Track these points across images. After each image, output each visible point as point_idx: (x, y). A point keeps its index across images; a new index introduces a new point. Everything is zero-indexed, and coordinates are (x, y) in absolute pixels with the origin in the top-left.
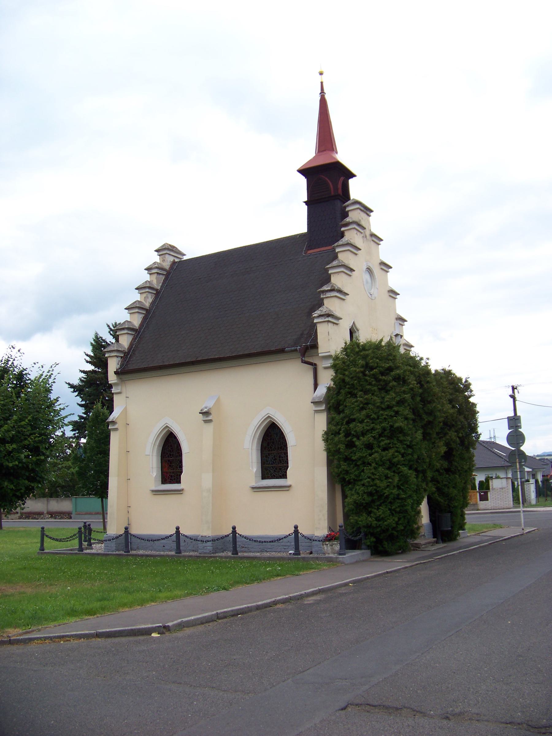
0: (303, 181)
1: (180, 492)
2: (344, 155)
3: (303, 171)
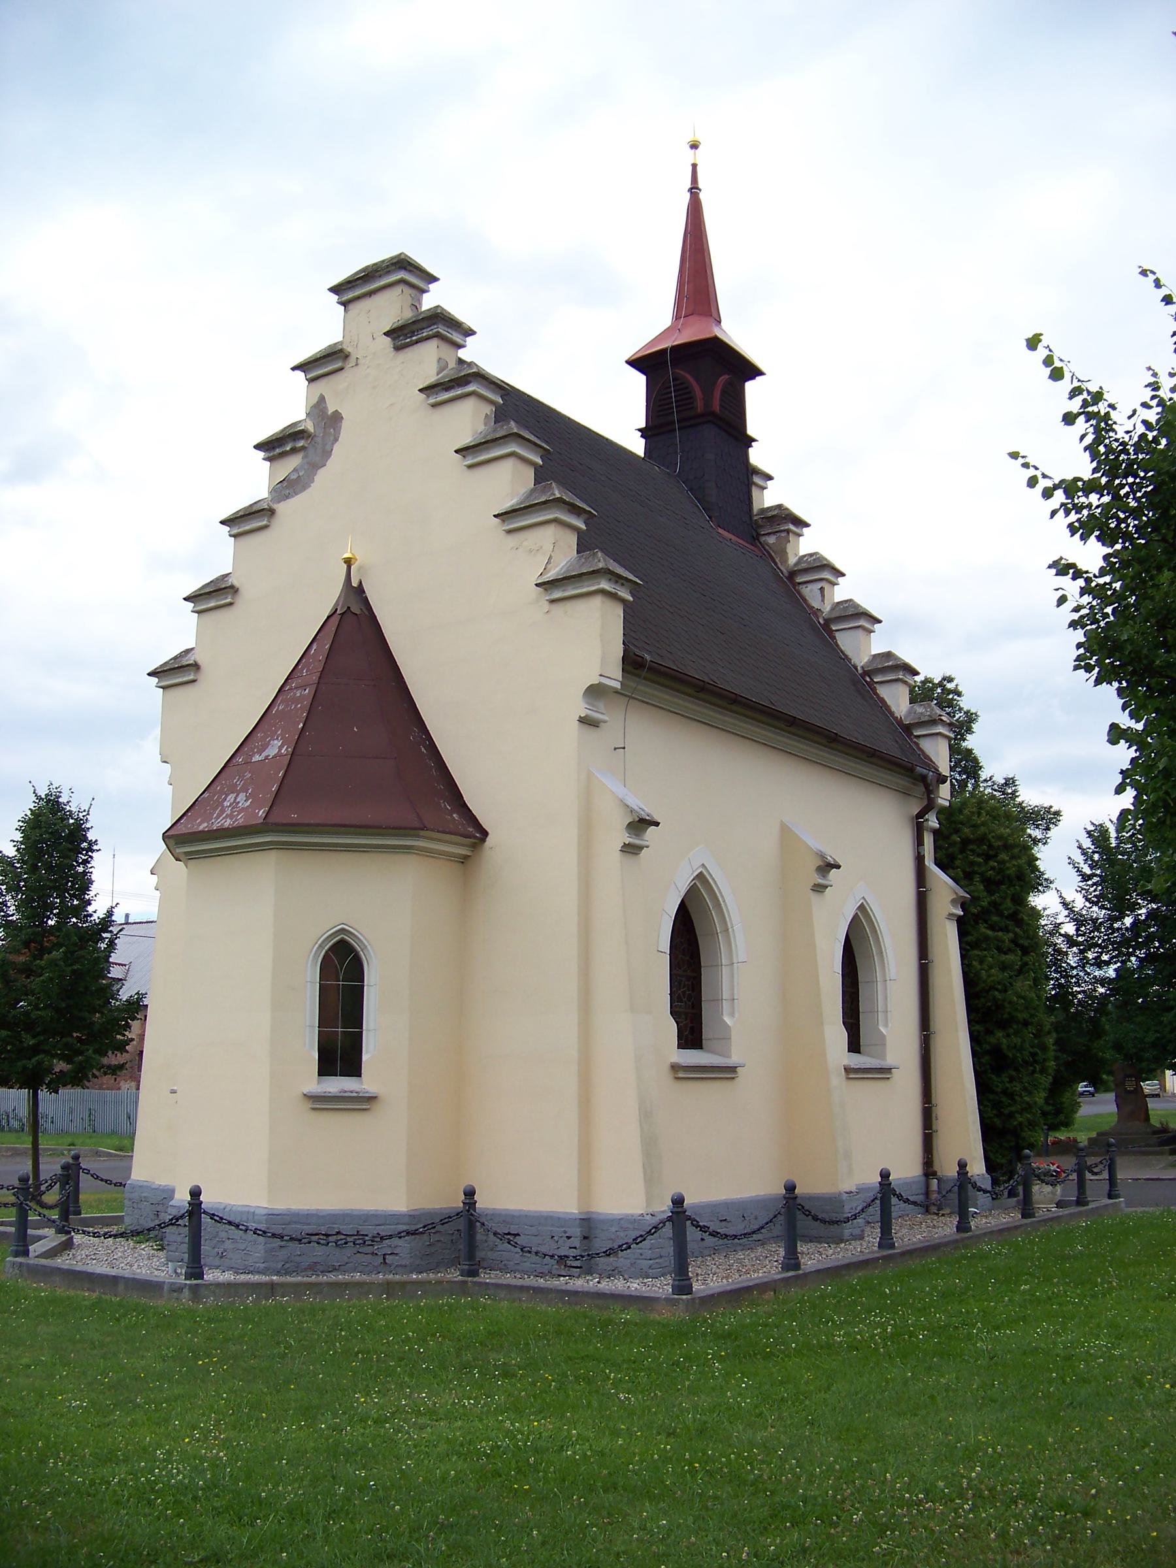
0: (638, 381)
1: (366, 1102)
2: (738, 329)
3: (636, 363)
